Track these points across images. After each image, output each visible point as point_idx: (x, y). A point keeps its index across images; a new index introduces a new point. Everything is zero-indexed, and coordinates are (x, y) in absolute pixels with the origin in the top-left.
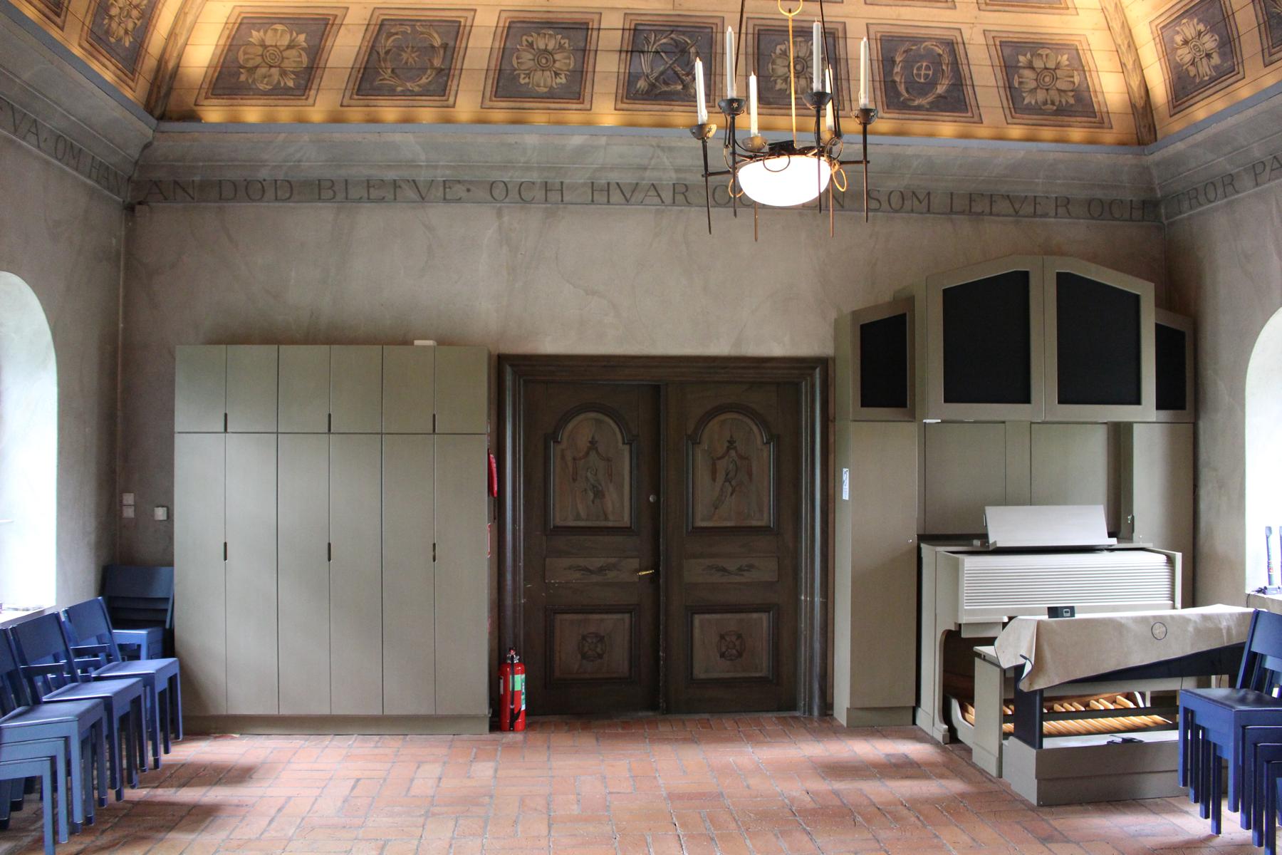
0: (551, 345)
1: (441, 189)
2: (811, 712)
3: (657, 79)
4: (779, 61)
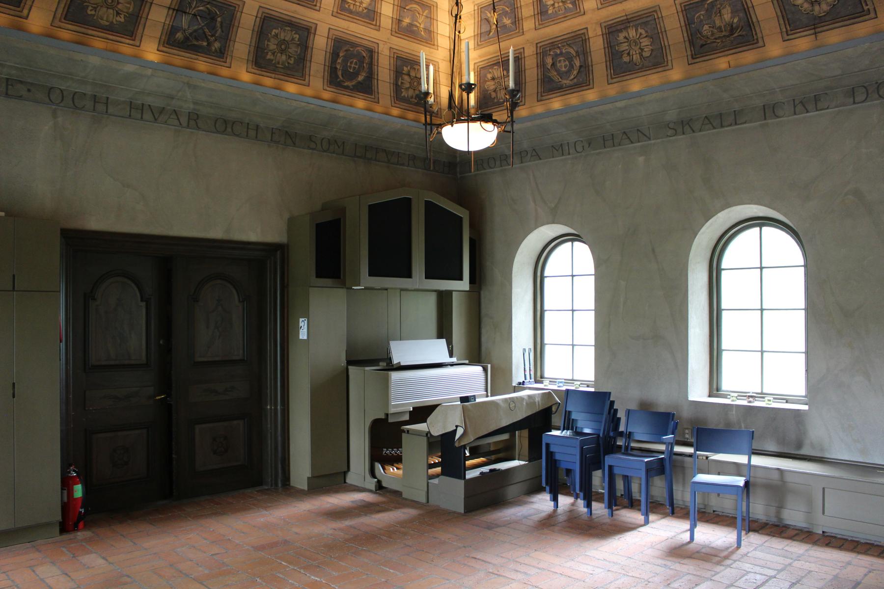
0: (95, 224)
1: (4, 85)
2: (276, 485)
3: (191, 34)
4: (272, 40)
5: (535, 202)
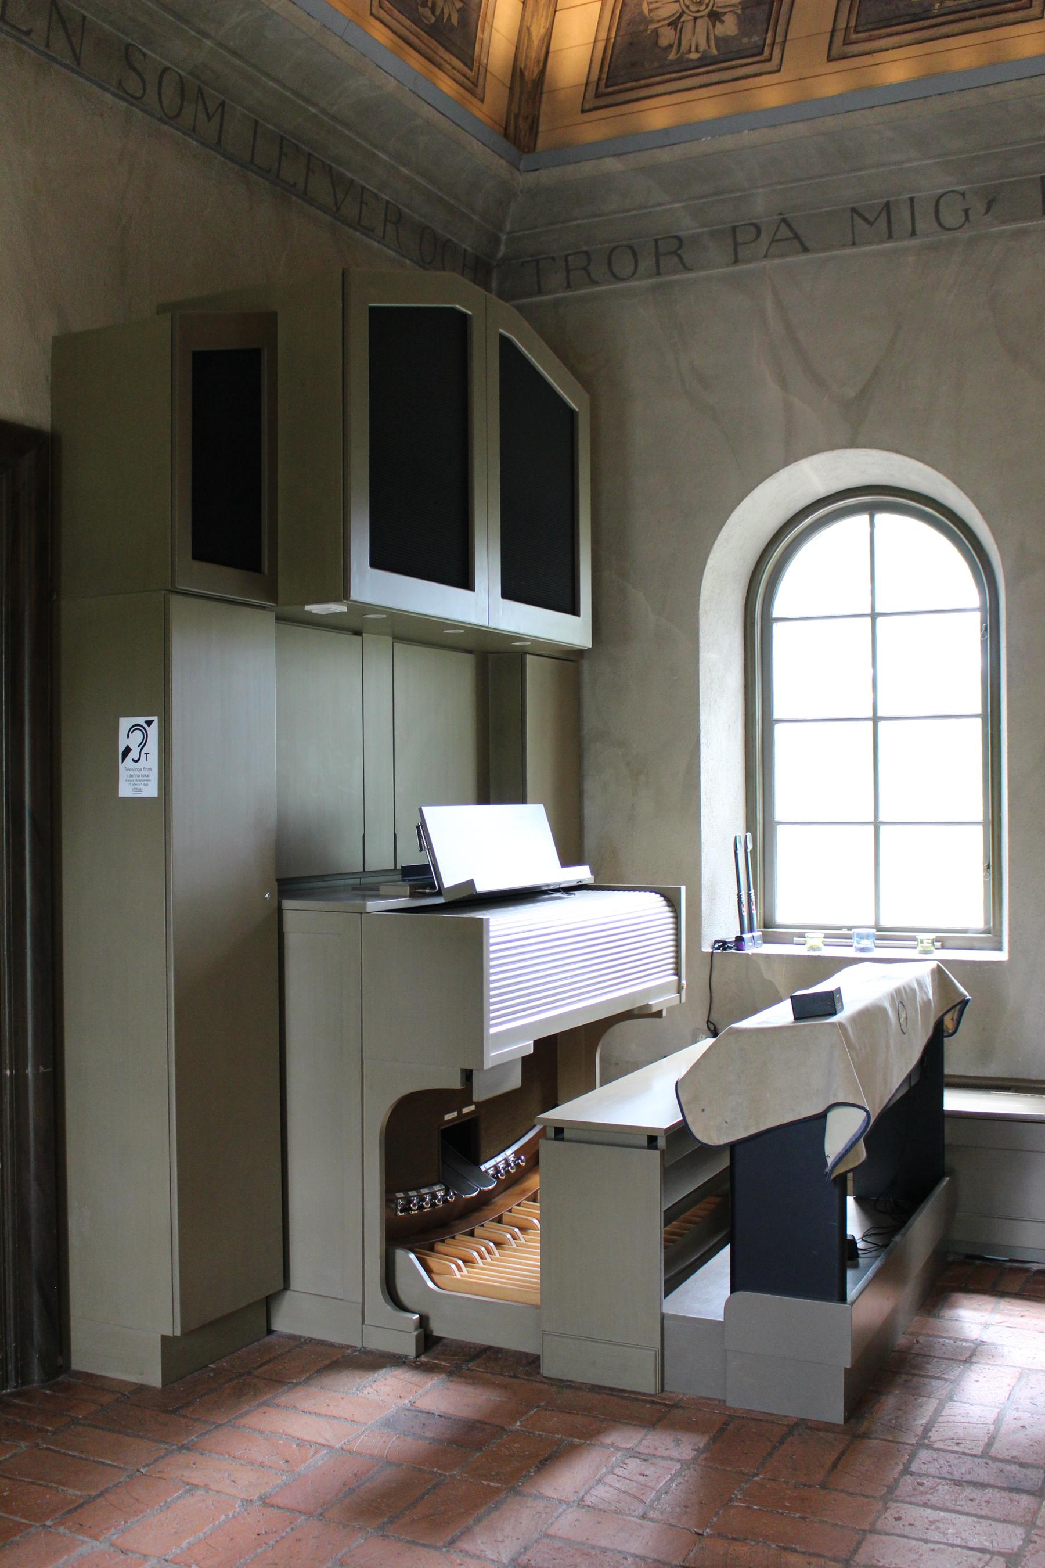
5: (783, 383)
